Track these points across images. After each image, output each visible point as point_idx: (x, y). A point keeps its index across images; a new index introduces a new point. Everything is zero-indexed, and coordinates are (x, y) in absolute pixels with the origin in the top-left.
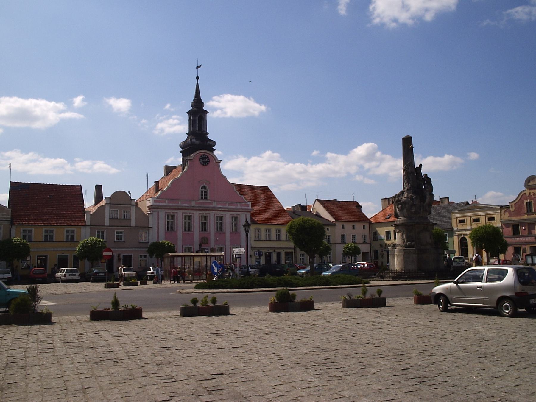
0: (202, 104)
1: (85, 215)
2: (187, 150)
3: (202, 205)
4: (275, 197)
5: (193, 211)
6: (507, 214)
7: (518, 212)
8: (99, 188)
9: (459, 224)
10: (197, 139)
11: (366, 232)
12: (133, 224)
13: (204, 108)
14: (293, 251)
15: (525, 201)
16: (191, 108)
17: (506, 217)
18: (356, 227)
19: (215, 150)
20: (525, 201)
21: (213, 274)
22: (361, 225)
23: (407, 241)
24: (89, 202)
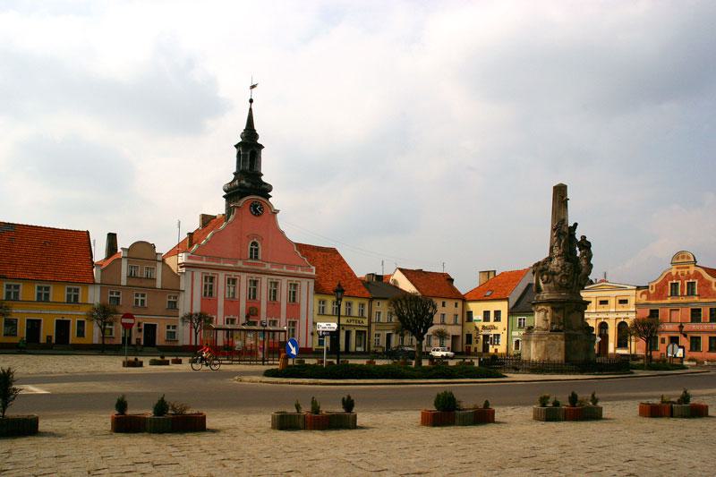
0: (256, 136)
1: (94, 270)
2: (232, 194)
3: (255, 267)
4: (345, 262)
5: (239, 274)
6: (645, 296)
7: (660, 293)
8: (112, 238)
9: (618, 304)
10: (247, 181)
11: (459, 310)
12: (159, 285)
13: (259, 141)
14: (366, 329)
15: (670, 282)
16: (241, 140)
17: (644, 299)
18: (446, 305)
19: (271, 196)
20: (670, 282)
21: (289, 356)
22: (453, 302)
23: (552, 324)
24: (99, 253)
